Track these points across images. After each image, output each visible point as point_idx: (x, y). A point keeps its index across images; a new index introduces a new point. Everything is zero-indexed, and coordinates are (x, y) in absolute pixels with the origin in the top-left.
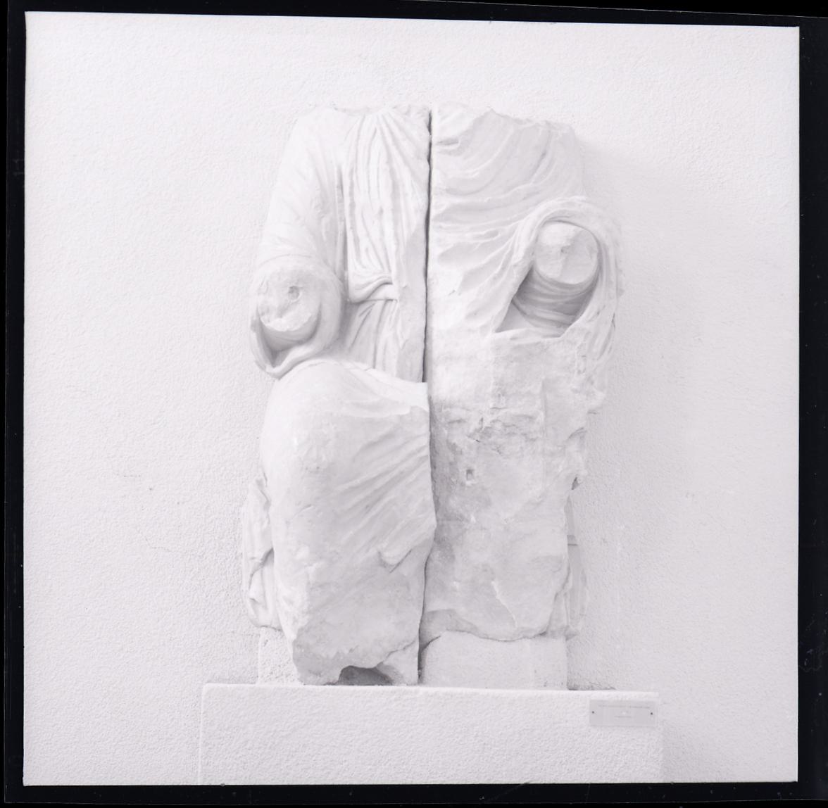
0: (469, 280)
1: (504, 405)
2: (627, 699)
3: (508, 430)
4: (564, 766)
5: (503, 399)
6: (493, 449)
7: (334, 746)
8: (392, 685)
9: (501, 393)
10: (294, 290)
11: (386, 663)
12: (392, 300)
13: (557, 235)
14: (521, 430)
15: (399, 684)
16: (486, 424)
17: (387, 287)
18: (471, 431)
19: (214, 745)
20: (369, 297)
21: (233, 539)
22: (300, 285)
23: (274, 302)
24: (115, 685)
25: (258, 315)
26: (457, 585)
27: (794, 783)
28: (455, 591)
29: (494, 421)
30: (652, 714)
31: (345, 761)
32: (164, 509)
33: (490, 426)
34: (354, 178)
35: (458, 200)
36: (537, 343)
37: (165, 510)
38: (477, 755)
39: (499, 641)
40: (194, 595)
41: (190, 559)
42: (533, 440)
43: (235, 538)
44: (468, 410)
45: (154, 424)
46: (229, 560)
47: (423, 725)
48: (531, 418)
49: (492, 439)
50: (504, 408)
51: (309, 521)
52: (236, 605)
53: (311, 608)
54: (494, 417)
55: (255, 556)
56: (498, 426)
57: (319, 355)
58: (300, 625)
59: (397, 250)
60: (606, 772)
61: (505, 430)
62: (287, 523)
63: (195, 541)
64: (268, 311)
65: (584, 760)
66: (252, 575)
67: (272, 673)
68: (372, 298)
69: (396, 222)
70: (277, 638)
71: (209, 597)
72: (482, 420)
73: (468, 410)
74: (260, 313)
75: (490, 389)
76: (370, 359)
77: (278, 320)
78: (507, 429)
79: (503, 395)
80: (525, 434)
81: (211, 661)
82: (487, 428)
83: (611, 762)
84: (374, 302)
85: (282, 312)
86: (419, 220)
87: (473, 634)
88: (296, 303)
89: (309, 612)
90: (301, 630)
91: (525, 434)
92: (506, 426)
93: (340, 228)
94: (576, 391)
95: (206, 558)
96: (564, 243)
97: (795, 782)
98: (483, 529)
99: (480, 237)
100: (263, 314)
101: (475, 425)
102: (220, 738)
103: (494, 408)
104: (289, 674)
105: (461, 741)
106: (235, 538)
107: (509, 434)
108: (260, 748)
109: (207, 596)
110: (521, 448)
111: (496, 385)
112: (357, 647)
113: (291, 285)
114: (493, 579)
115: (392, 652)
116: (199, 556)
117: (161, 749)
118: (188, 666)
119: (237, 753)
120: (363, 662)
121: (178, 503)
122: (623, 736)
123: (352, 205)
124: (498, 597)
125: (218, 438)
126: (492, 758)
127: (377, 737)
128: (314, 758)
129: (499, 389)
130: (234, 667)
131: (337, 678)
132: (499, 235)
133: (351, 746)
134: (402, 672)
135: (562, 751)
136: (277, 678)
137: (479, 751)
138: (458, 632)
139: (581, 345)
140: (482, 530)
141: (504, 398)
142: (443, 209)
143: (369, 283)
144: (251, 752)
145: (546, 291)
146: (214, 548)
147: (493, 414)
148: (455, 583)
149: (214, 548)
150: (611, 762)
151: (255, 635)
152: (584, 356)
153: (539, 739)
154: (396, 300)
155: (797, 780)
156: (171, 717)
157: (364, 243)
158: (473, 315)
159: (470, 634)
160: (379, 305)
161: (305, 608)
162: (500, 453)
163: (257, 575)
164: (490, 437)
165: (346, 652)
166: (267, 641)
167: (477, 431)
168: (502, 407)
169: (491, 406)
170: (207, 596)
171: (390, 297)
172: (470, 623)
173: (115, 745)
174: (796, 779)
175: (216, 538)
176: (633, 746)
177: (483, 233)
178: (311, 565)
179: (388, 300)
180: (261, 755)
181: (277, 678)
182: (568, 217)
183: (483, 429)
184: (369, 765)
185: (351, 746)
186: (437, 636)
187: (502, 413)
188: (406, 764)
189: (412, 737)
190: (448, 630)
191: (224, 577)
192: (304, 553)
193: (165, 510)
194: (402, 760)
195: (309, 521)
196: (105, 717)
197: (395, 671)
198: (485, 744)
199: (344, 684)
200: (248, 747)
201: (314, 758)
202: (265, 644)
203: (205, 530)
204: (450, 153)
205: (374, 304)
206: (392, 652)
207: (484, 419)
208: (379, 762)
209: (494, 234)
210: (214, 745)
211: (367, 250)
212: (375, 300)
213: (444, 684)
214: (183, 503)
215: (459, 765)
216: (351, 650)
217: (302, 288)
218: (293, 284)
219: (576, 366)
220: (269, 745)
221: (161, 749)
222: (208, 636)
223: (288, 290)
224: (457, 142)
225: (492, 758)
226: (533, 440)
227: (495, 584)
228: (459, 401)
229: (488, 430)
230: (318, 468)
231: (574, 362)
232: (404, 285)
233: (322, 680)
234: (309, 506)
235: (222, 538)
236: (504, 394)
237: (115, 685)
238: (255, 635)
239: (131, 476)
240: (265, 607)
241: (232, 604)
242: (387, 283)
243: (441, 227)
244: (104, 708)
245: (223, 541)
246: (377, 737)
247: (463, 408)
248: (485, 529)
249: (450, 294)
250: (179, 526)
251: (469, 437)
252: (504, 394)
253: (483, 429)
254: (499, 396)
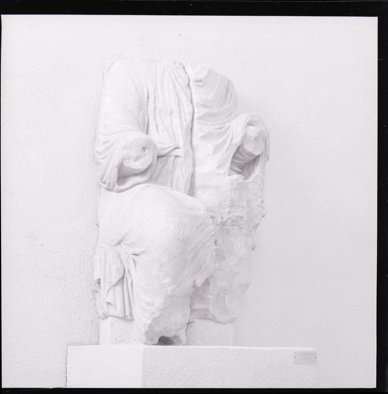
0: (217, 149)
1: (233, 211)
2: (307, 351)
3: (233, 223)
4: (284, 382)
5: (233, 208)
6: (226, 232)
7: (197, 375)
8: (175, 345)
9: (232, 205)
10: (144, 149)
11: (176, 335)
12: (178, 157)
13: (253, 131)
14: (238, 223)
15: (178, 345)
16: (224, 220)
17: (177, 150)
18: (218, 223)
19: (148, 376)
20: (166, 154)
21: (79, 272)
22: (147, 147)
23: (134, 153)
24: (25, 347)
25: (123, 160)
26: (210, 297)
27: (374, 389)
28: (209, 299)
29: (228, 219)
30: (295, 357)
31: (201, 382)
32: (48, 255)
33: (226, 221)
34: (156, 94)
35: (207, 110)
36: (243, 182)
37: (48, 256)
38: (252, 378)
39: (222, 323)
40: (62, 300)
41: (60, 282)
42: (242, 228)
43: (80, 271)
44: (214, 212)
45: (43, 211)
46: (77, 282)
47: (232, 364)
48: (242, 218)
49: (226, 227)
50: (233, 212)
51: (174, 265)
52: (80, 305)
53: (164, 308)
54: (228, 217)
55: (113, 281)
56: (230, 221)
57: (146, 182)
58: (155, 316)
59: (182, 133)
60: (300, 384)
61: (232, 223)
62: (161, 265)
63: (63, 272)
64: (129, 158)
65: (291, 379)
66: (108, 291)
67: (116, 340)
68: (168, 155)
69: (180, 117)
70: (118, 322)
71: (69, 301)
72: (222, 218)
73: (214, 212)
74: (124, 159)
75: (228, 203)
76: (170, 185)
77: (134, 163)
78: (233, 223)
79: (233, 206)
80: (239, 225)
81: (70, 334)
82: (225, 221)
83: (301, 380)
84: (169, 157)
85: (137, 159)
86: (189, 118)
87: (212, 321)
88: (145, 155)
89: (162, 310)
90: (155, 319)
91: (239, 225)
92: (232, 221)
93: (147, 118)
94: (258, 206)
95: (67, 281)
96: (256, 135)
97: (375, 388)
98: (222, 270)
99: (217, 129)
100: (126, 159)
101: (220, 220)
102: (150, 373)
103: (229, 212)
104: (125, 340)
105: (246, 371)
106: (80, 271)
107: (233, 225)
108: (167, 377)
109: (68, 301)
110: (237, 232)
111: (231, 201)
112: (167, 327)
113: (143, 146)
114: (226, 294)
115: (179, 329)
116: (64, 280)
117: (47, 379)
118: (59, 336)
119: (157, 380)
120: (169, 334)
121: (54, 253)
122: (305, 368)
123: (155, 108)
124: (226, 303)
125: (72, 220)
126: (258, 379)
127: (214, 371)
128: (189, 382)
129: (232, 203)
130: (79, 336)
131: (157, 342)
132: (224, 129)
133: (204, 375)
134: (181, 339)
135: (283, 375)
136: (118, 342)
137: (253, 376)
138: (204, 320)
139: (260, 184)
140: (221, 270)
141: (233, 207)
142: (202, 114)
143: (169, 147)
144: (163, 379)
145: (241, 157)
146: (71, 276)
147: (228, 215)
148: (209, 295)
149: (71, 276)
150: (301, 380)
151: (89, 321)
152: (261, 189)
153: (275, 370)
154: (182, 157)
155: (376, 387)
156: (52, 363)
157: (161, 127)
158: (219, 167)
159: (210, 321)
160: (172, 159)
161: (161, 307)
162: (228, 234)
163: (112, 290)
164: (225, 226)
165: (162, 329)
166: (113, 323)
167: (220, 222)
168: (232, 212)
169: (228, 211)
170: (68, 301)
171: (178, 155)
172: (213, 315)
173: (26, 378)
174: (376, 387)
175: (72, 271)
176: (309, 372)
177: (218, 127)
178: (169, 286)
179: (177, 156)
180: (167, 380)
181: (118, 342)
182: (253, 123)
183: (223, 222)
184: (211, 384)
185: (204, 375)
186: (192, 321)
187: (232, 215)
188: (225, 383)
189: (228, 370)
190: (198, 318)
191: (75, 291)
192: (167, 280)
193: (48, 256)
194: (224, 381)
195: (174, 265)
196: (21, 363)
197: (179, 338)
198: (255, 373)
199: (160, 345)
200: (162, 376)
201: (189, 382)
202: (112, 325)
203: (67, 267)
204: (199, 86)
205: (169, 158)
206: (179, 329)
207: (223, 217)
208: (215, 383)
209: (221, 128)
210: (148, 376)
211: (163, 131)
212: (170, 156)
213: (198, 344)
214: (57, 252)
215: (246, 383)
216: (164, 328)
217: (148, 148)
218: (144, 146)
219: (258, 194)
220: (171, 375)
221: (47, 379)
222: (68, 321)
223: (141, 148)
224: (202, 82)
225: (258, 379)
226: (242, 228)
227: (226, 296)
228: (210, 208)
229: (225, 223)
230: (183, 239)
231: (257, 192)
232: (186, 150)
233: (153, 343)
234: (176, 257)
235: (75, 271)
236: (233, 206)
237: (25, 347)
238: (89, 321)
239: (33, 238)
240: (116, 307)
241: (79, 305)
242: (176, 148)
243: (200, 123)
244: (20, 359)
245: (75, 272)
246: (214, 371)
247: (212, 211)
248: (223, 270)
249: (207, 156)
250: (55, 265)
251: (217, 225)
252: (233, 206)
253: (223, 222)
254: (231, 206)
